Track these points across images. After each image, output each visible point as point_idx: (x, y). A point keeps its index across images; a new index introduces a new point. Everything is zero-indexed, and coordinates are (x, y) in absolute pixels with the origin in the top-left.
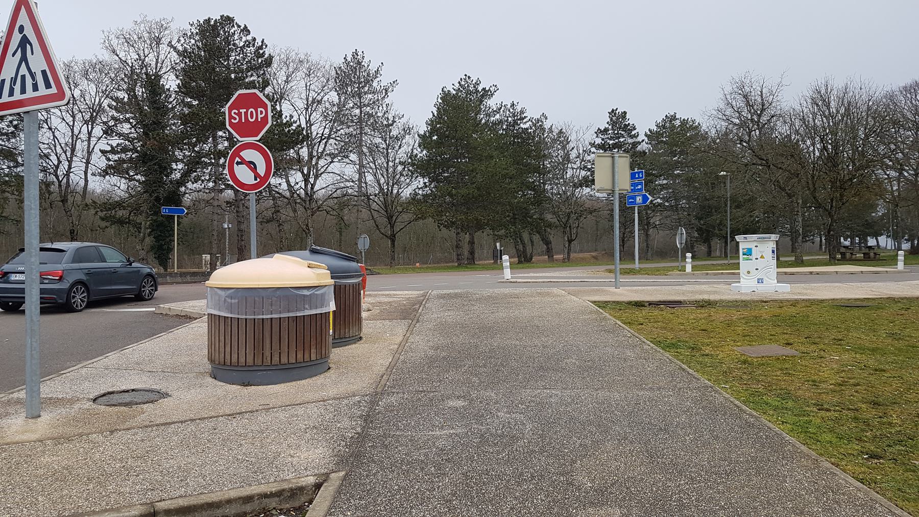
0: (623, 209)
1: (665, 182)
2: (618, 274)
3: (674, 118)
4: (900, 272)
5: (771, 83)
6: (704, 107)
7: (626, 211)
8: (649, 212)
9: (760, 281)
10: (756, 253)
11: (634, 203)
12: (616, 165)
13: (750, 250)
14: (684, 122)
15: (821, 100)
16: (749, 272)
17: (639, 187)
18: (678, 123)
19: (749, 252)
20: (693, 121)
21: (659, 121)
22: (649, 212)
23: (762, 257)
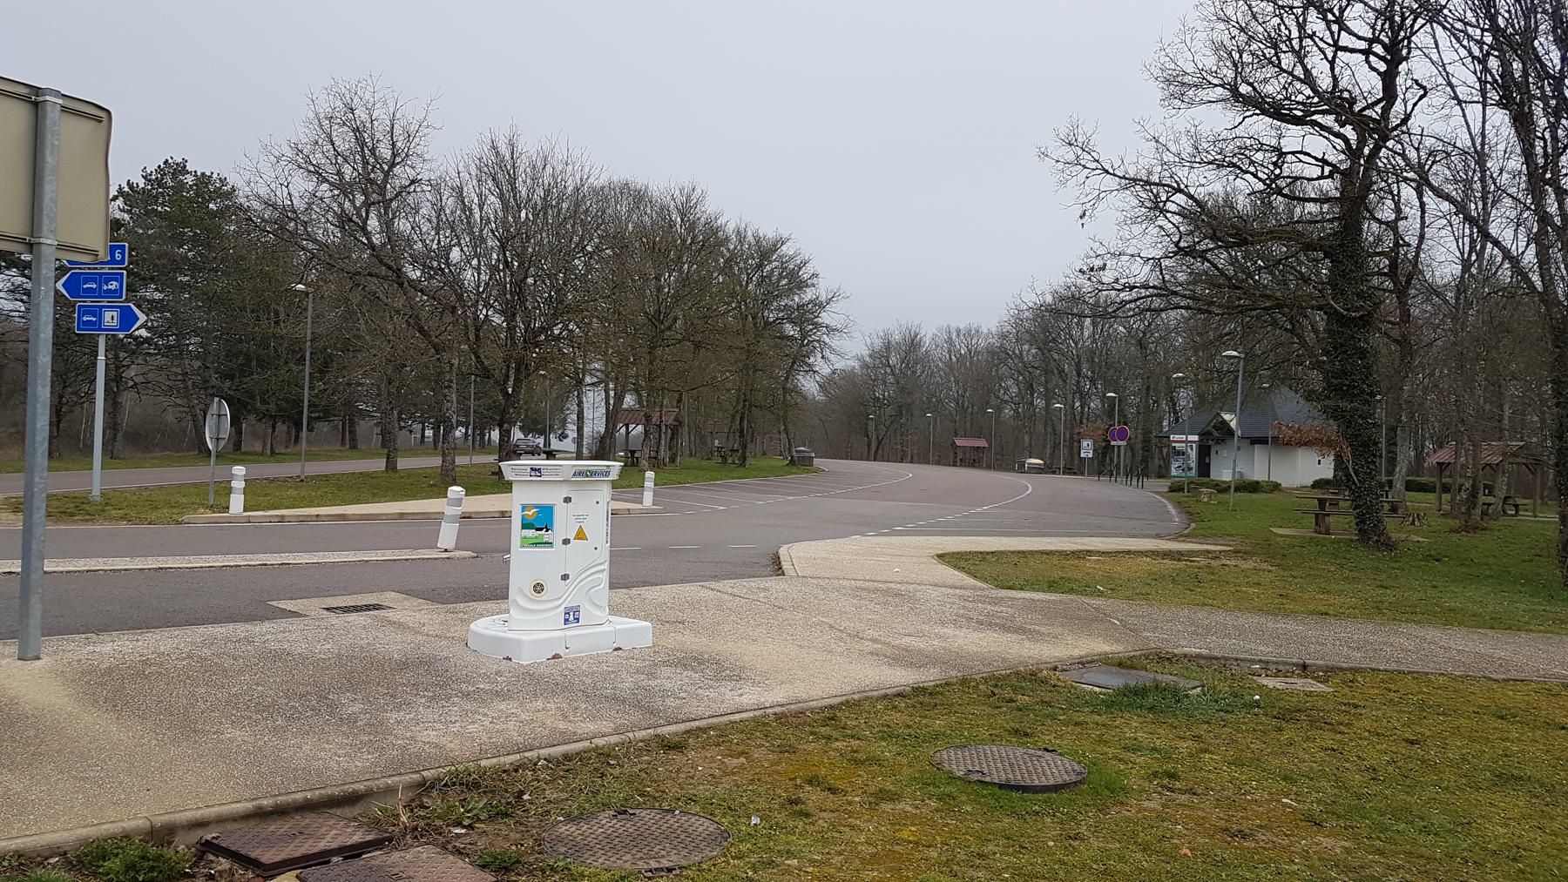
0: (64, 341)
1: (157, 296)
2: (39, 515)
3: (181, 169)
4: (647, 512)
5: (410, 114)
6: (252, 149)
7: (72, 349)
8: (122, 355)
9: (572, 616)
10: (563, 524)
11: (98, 325)
12: (50, 140)
13: (547, 511)
14: (203, 180)
15: (500, 171)
16: (538, 588)
17: (113, 285)
18: (189, 179)
19: (540, 521)
20: (223, 181)
21: (151, 168)
22: (122, 355)
23: (581, 535)
